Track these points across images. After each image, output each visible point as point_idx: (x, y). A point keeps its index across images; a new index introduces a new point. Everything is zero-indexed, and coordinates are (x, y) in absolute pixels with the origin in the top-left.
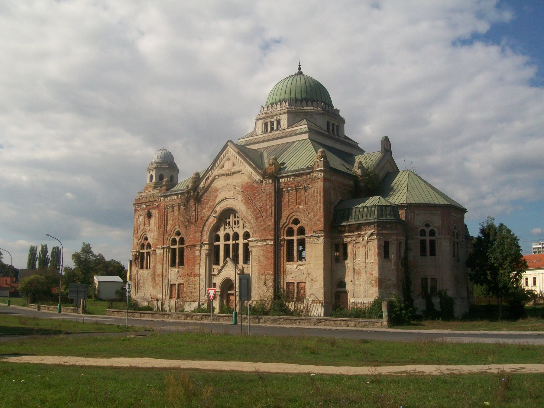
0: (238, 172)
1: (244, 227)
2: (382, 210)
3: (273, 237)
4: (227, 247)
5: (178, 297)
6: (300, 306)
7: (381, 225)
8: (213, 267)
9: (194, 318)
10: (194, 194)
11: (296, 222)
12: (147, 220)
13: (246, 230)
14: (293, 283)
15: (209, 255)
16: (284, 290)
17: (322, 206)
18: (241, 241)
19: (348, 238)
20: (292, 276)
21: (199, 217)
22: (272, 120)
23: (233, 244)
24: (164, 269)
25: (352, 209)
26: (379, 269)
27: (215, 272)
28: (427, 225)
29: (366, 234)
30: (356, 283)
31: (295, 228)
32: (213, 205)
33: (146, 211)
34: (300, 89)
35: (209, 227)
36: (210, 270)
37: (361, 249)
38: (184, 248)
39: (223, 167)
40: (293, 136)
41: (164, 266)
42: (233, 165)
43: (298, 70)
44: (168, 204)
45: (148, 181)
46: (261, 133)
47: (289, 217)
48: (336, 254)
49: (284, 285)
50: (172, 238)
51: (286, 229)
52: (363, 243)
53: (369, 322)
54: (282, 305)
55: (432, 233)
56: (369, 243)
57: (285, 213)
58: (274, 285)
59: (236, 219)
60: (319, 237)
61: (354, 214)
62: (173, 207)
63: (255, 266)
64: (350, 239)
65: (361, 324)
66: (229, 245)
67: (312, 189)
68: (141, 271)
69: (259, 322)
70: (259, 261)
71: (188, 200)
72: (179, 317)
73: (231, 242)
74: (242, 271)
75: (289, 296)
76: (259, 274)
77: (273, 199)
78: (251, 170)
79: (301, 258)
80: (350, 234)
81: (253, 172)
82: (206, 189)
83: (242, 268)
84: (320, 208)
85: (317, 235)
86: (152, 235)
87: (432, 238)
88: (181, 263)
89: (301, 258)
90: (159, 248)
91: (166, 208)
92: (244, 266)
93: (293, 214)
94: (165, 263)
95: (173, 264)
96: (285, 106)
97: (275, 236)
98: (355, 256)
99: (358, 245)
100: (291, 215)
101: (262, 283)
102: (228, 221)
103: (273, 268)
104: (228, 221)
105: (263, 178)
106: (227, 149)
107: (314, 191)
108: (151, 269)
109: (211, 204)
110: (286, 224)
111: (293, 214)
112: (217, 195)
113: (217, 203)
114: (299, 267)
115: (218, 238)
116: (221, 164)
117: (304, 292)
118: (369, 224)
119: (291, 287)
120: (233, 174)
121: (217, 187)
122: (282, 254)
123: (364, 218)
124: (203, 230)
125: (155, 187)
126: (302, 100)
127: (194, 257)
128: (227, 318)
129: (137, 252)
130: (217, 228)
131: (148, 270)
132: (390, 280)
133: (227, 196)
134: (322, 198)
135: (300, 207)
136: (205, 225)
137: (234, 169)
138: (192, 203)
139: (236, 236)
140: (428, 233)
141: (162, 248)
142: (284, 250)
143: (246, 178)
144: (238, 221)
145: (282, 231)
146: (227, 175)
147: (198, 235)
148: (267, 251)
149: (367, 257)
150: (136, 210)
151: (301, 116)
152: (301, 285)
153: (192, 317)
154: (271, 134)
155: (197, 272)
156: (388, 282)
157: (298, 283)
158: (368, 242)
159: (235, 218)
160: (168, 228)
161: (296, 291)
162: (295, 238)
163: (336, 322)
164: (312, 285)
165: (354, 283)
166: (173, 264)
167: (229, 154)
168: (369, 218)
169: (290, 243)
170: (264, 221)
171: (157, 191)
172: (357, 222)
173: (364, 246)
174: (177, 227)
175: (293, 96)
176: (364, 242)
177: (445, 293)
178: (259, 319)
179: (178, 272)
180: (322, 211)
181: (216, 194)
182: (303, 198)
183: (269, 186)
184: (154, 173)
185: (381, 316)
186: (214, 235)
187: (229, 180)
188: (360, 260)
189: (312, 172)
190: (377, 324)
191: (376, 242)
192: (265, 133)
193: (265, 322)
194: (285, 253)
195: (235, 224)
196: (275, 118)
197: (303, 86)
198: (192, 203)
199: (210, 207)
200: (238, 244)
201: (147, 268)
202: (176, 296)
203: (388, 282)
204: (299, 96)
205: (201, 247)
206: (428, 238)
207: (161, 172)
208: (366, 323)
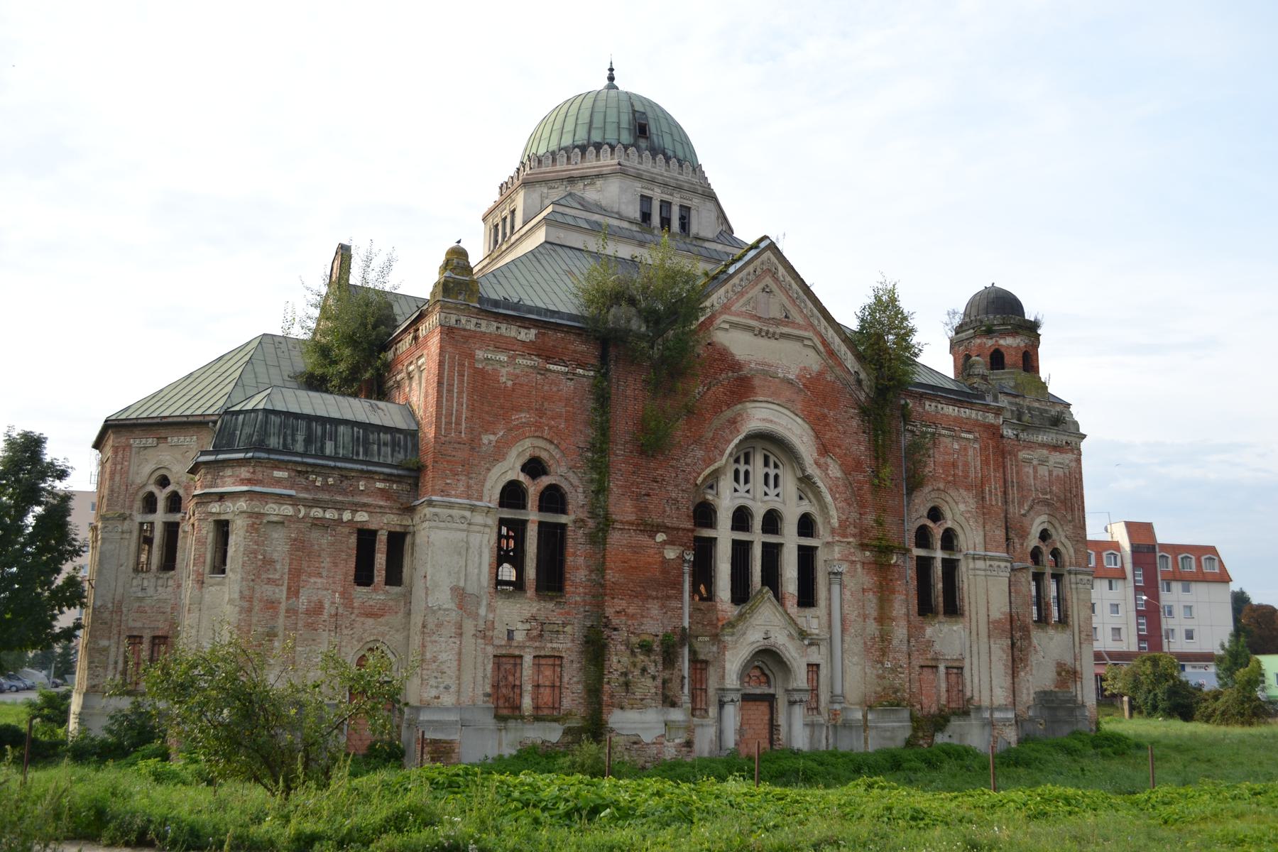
4: (741, 551)
18: (790, 541)
38: (563, 526)
43: (607, 82)
50: (917, 524)
139: (772, 521)
140: (161, 505)
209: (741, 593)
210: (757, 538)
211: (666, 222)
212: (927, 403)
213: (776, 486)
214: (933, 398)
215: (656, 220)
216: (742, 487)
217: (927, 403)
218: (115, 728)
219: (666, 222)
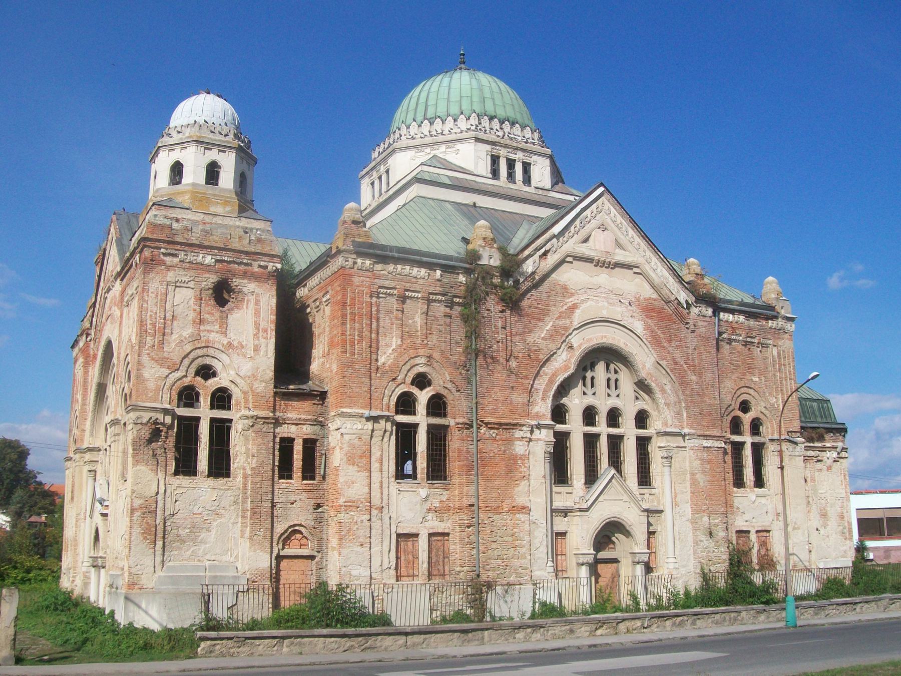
0: (628, 267)
4: (591, 441)
11: (206, 372)
12: (211, 311)
18: (628, 430)
20: (746, 517)
22: (512, 156)
24: (375, 486)
33: (213, 279)
35: (551, 381)
39: (586, 240)
44: (387, 283)
47: (736, 395)
50: (399, 391)
70: (694, 482)
72: (572, 631)
78: (666, 273)
88: (437, 470)
104: (589, 374)
113: (576, 324)
116: (583, 234)
128: (718, 617)
129: (166, 412)
130: (564, 389)
133: (605, 314)
137: (620, 256)
138: (492, 305)
141: (368, 419)
148: (710, 462)
155: (520, 500)
160: (382, 360)
174: (423, 360)
179: (426, 499)
181: (570, 301)
187: (603, 278)
209: (591, 476)
210: (602, 428)
211: (511, 164)
212: (722, 314)
213: (592, 386)
214: (396, 261)
215: (519, 168)
216: (613, 393)
217: (722, 314)
218: (349, 591)
219: (511, 164)
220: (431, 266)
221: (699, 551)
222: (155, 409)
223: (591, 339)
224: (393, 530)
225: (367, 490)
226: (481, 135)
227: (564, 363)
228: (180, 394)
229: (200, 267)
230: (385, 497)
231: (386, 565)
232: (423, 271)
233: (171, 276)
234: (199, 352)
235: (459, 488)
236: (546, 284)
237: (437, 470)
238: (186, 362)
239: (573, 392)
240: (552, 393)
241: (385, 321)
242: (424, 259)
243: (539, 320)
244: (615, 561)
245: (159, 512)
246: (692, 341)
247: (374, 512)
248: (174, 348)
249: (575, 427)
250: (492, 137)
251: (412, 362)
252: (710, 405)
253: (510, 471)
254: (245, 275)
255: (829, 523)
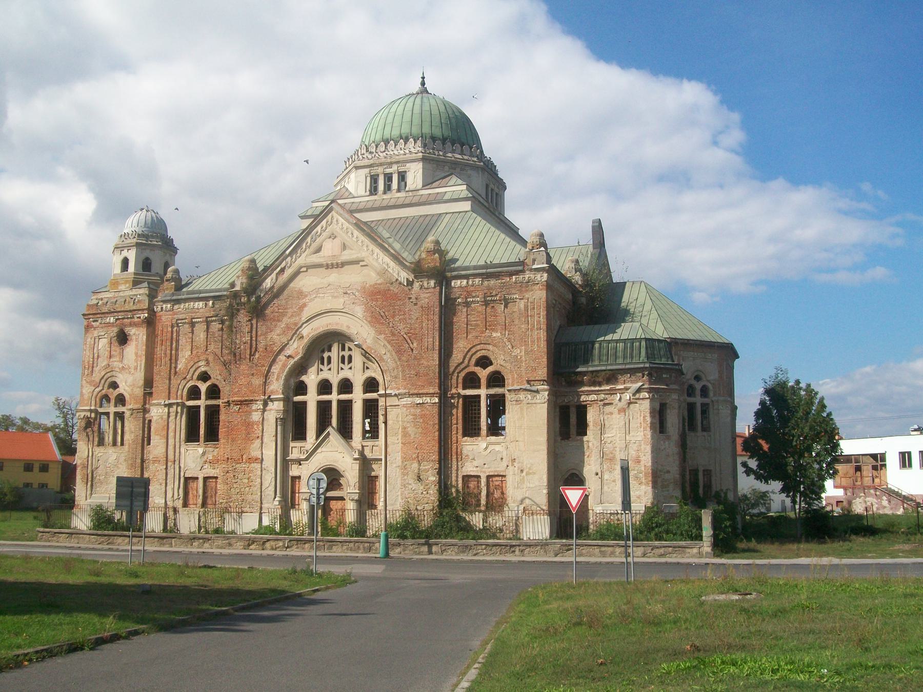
1: (366, 368)
2: (653, 347)
3: (437, 390)
4: (324, 409)
5: (204, 504)
6: (496, 521)
7: (655, 373)
8: (292, 444)
9: (268, 545)
10: (249, 300)
11: (484, 362)
12: (116, 348)
13: (369, 374)
14: (479, 477)
15: (282, 421)
16: (457, 491)
17: (543, 335)
18: (358, 397)
19: (588, 395)
20: (476, 463)
21: (261, 347)
22: (388, 171)
23: (340, 402)
24: (171, 448)
25: (593, 343)
26: (652, 452)
27: (294, 454)
28: (697, 378)
29: (627, 389)
30: (606, 477)
31: (483, 374)
32: (296, 324)
33: (116, 330)
34: (438, 119)
35: (284, 366)
36: (286, 451)
37: (616, 416)
39: (319, 250)
40: (439, 203)
41: (171, 441)
42: (344, 247)
44: (181, 316)
45: (117, 269)
46: (363, 193)
47: (470, 353)
48: (568, 423)
49: (457, 481)
50: (189, 385)
51: (462, 374)
52: (621, 405)
53: (674, 547)
54: (458, 519)
55: (704, 392)
56: (632, 406)
57: (460, 347)
58: (440, 482)
59: (346, 353)
60: (537, 391)
61: (596, 352)
62: (193, 325)
63: (393, 444)
64: (593, 397)
65: (657, 551)
66: (330, 402)
67: (522, 304)
68: (99, 451)
69: (430, 552)
70: (405, 434)
71: (232, 313)
72: (230, 545)
73: (334, 397)
74: (362, 453)
75: (469, 501)
76: (404, 459)
77: (437, 316)
78: (387, 259)
79: (495, 430)
80: (593, 388)
81: (392, 264)
82: (277, 293)
83: (360, 448)
84: (539, 339)
85: (534, 388)
86: (130, 379)
87: (705, 400)
88: (212, 435)
89: (495, 430)
90: (159, 404)
91: (176, 325)
92: (365, 444)
93: (478, 347)
94: (171, 434)
95: (192, 436)
96: (415, 148)
97: (440, 389)
98: (602, 428)
99: (608, 409)
100: (474, 350)
101: (411, 479)
102: (326, 355)
103: (436, 449)
104: (326, 355)
105: (415, 277)
106: (329, 217)
107: (526, 307)
108: (126, 447)
109: (293, 320)
110: (462, 367)
111: (478, 347)
112: (305, 305)
113: (304, 319)
114: (491, 448)
115: (301, 388)
116: (315, 246)
117: (503, 493)
118: (633, 372)
119: (472, 485)
120: (343, 264)
121: (304, 290)
122: (454, 422)
123: (620, 361)
124: (269, 371)
125: (136, 283)
126: (444, 140)
127: (249, 425)
128: (352, 545)
129: (91, 411)
130: (301, 368)
131: (119, 449)
132: (668, 472)
133: (328, 306)
134: (543, 320)
135: (494, 335)
136: (274, 361)
137: (347, 256)
138: (243, 317)
139: (346, 386)
142: (458, 414)
143: (373, 274)
144: (350, 357)
145: (455, 378)
146: (327, 267)
147: (257, 381)
149: (628, 431)
150: (88, 328)
151: (446, 168)
152: (496, 481)
153: (264, 543)
154: (385, 197)
155: (256, 453)
156: (667, 476)
157: (488, 477)
158: (630, 403)
159: (343, 349)
160: (179, 366)
161: (484, 493)
162: (483, 392)
163: (603, 549)
164: (522, 481)
165: (601, 478)
166: (192, 436)
167: (334, 228)
168: (629, 360)
169: (471, 403)
170: (415, 358)
171: (142, 291)
172: (609, 368)
173: (622, 411)
174: (202, 363)
175: (426, 130)
176: (623, 404)
177: (726, 494)
178: (430, 546)
179: (204, 454)
180: (543, 344)
181: (301, 302)
182: (501, 319)
183: (426, 292)
184: (132, 255)
185: (699, 537)
186: (292, 382)
187: (334, 277)
188: (614, 434)
189: (523, 271)
190: (688, 550)
191: (646, 405)
192: (371, 194)
193: (442, 552)
194: (460, 421)
195: (343, 362)
196: (395, 167)
197: (444, 116)
198: (243, 317)
199: (288, 327)
200: (350, 402)
201: (115, 444)
202: (200, 501)
203: (667, 476)
204: (437, 132)
205: (265, 404)
206: (698, 400)
207: (147, 253)
208: (666, 549)
220: (206, 299)
221: (406, 492)
222: (85, 410)
223: (318, 328)
224: (182, 474)
225: (164, 450)
226: (358, 163)
227: (296, 349)
228: (465, 379)
229: (109, 325)
230: (177, 454)
231: (176, 496)
232: (201, 303)
233: (96, 333)
234: (109, 375)
235: (223, 447)
236: (286, 292)
237: (212, 435)
238: (103, 382)
239: (310, 370)
240: (285, 373)
241: (183, 341)
242: (201, 295)
243: (279, 321)
244: (342, 499)
245: (89, 467)
246: (416, 313)
247: (169, 464)
248: (97, 376)
249: (312, 399)
250: (366, 162)
251: (196, 365)
252: (428, 367)
253: (249, 434)
254: (131, 325)
255: (752, 477)
